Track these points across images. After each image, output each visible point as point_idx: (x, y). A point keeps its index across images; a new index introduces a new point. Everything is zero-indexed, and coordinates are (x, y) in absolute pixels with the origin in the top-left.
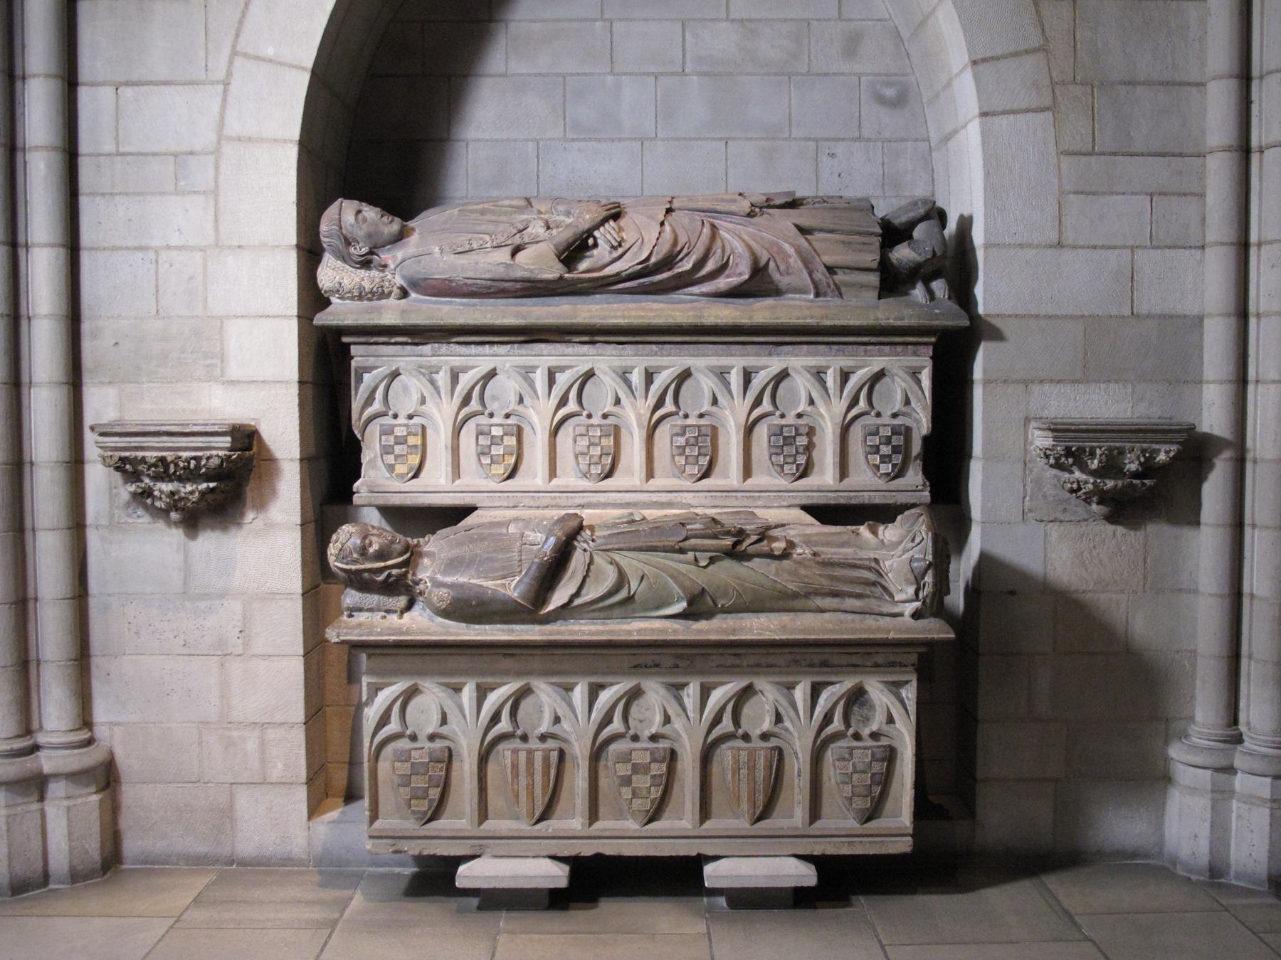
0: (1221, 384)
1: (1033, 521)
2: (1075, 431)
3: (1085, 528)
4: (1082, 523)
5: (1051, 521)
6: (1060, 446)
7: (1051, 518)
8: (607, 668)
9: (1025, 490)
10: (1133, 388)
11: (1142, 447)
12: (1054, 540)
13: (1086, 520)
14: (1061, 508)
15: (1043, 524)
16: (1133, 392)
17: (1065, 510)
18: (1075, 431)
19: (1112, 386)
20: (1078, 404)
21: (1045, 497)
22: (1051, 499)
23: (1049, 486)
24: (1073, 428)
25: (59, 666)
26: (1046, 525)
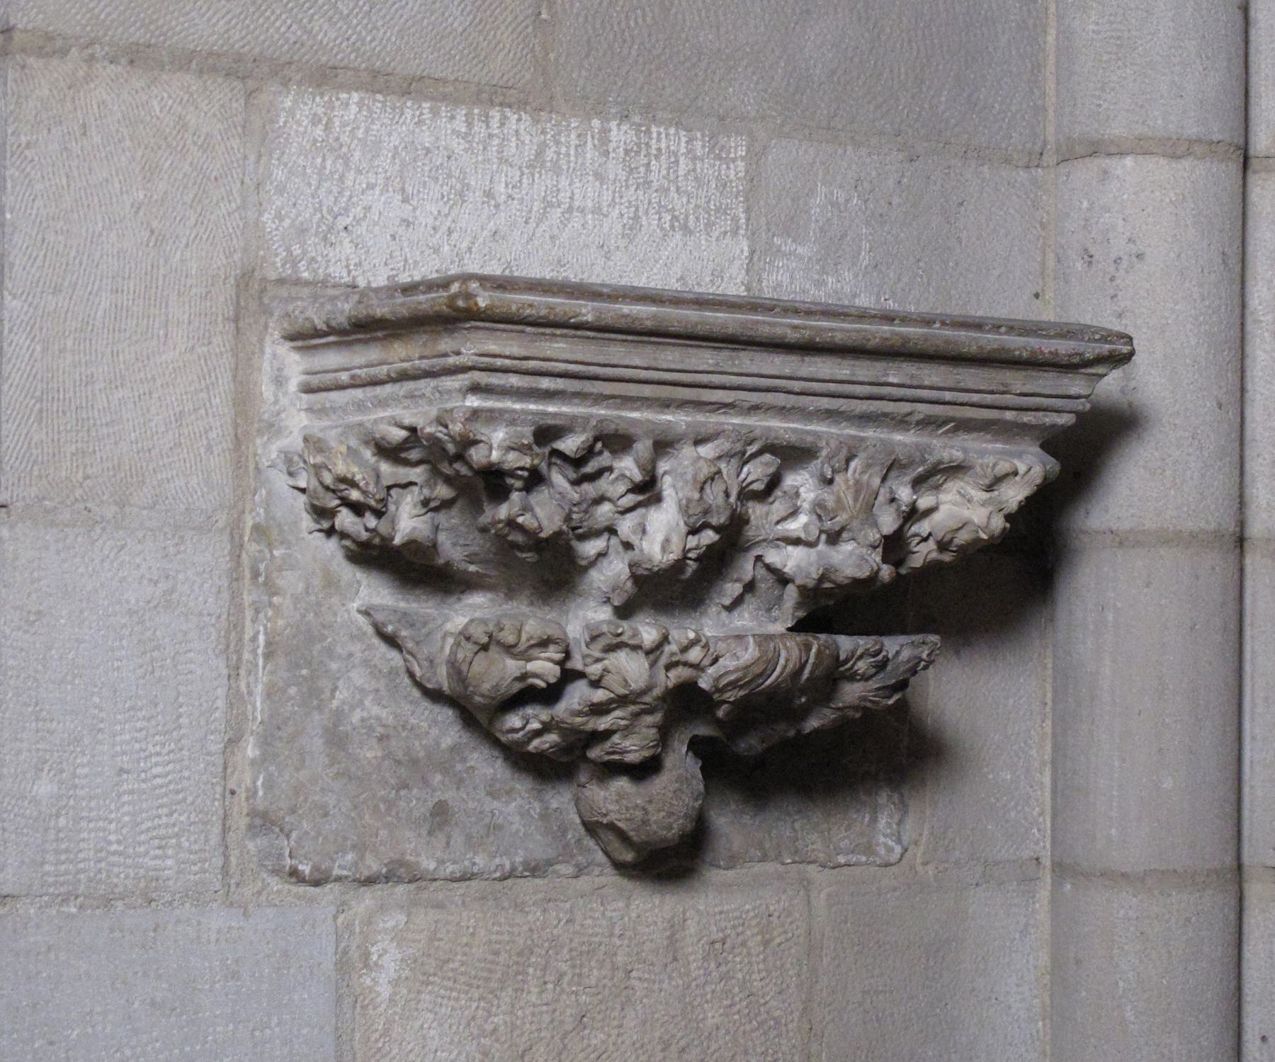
0: (1175, 157)
1: (275, 884)
2: (603, 329)
3: (535, 915)
4: (529, 888)
5: (370, 881)
6: (512, 419)
7: (373, 865)
8: (36, 448)
9: (236, 700)
10: (755, 156)
11: (888, 447)
12: (385, 991)
13: (535, 870)
14: (417, 802)
15: (329, 892)
16: (753, 180)
17: (441, 815)
18: (603, 329)
19: (667, 139)
20: (502, 219)
21: (336, 740)
22: (371, 753)
23: (358, 677)
24: (587, 311)
25: (748, 541)
26: (342, 907)
